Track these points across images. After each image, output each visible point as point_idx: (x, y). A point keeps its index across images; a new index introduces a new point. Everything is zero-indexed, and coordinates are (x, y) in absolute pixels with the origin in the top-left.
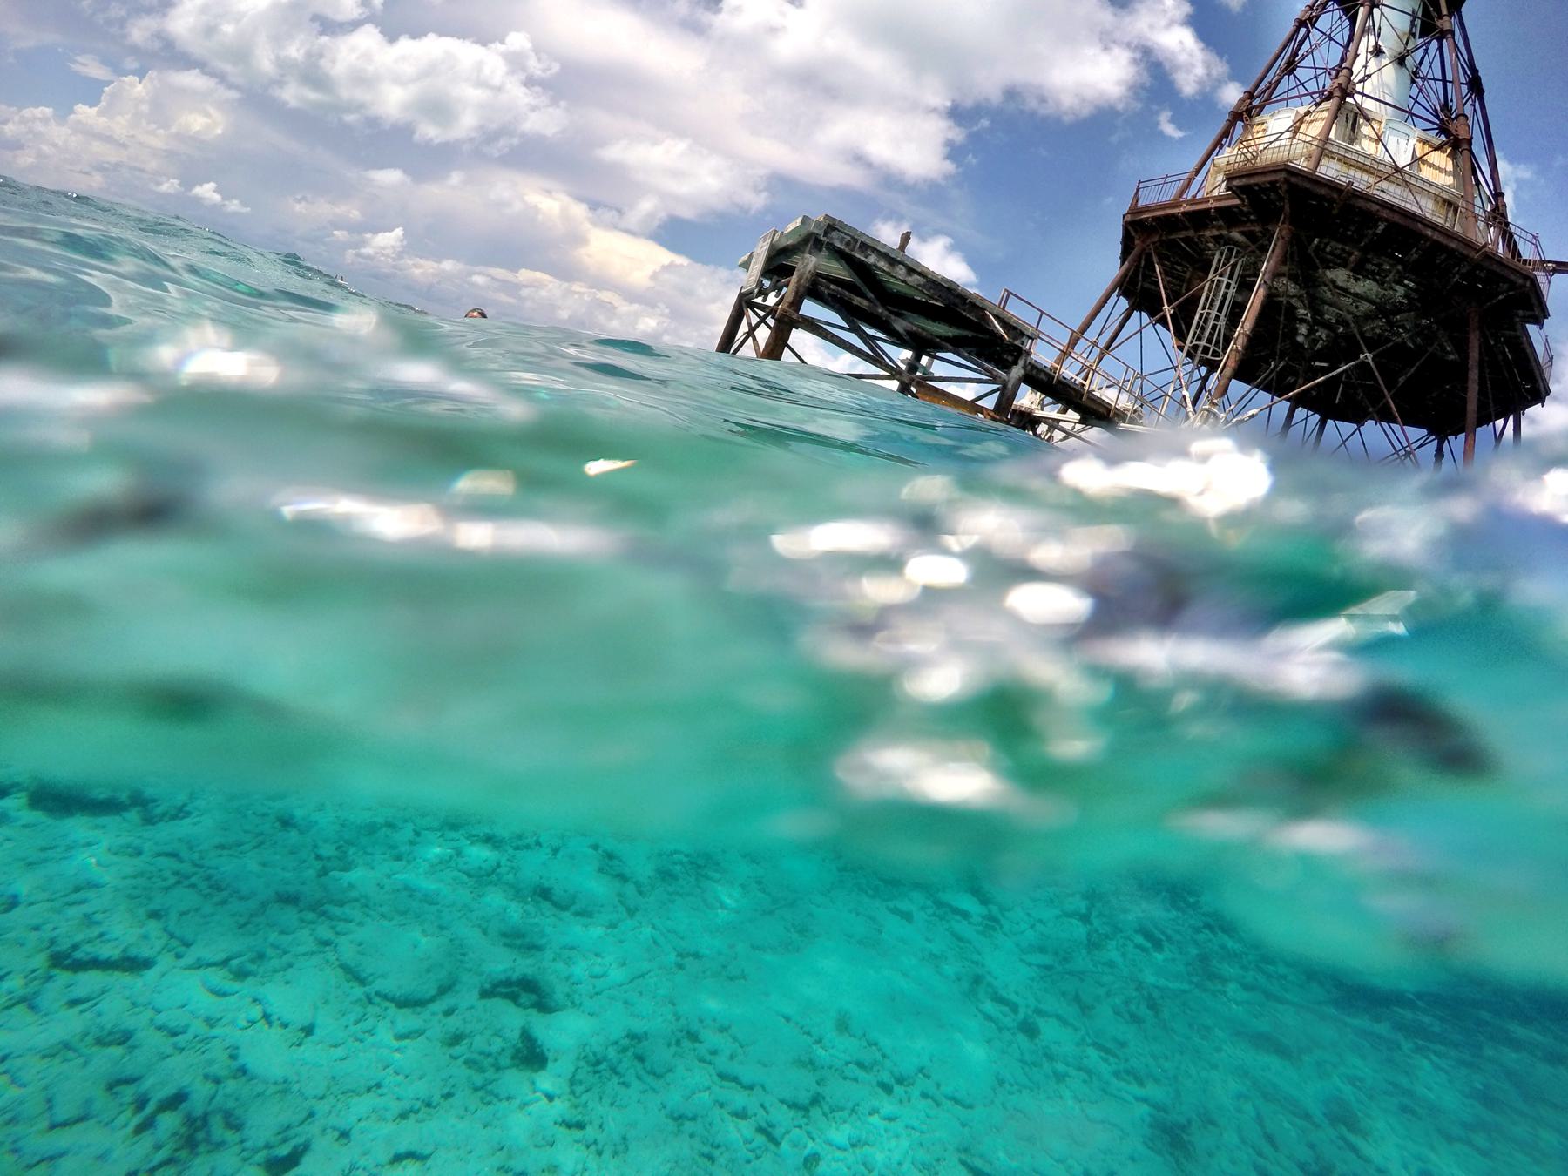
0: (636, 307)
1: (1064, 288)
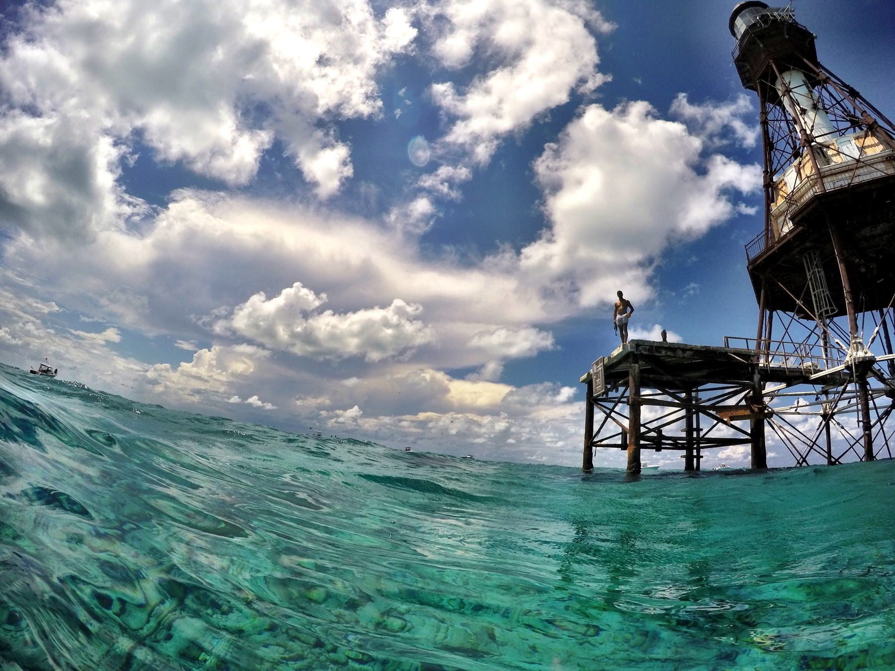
1: (732, 320)
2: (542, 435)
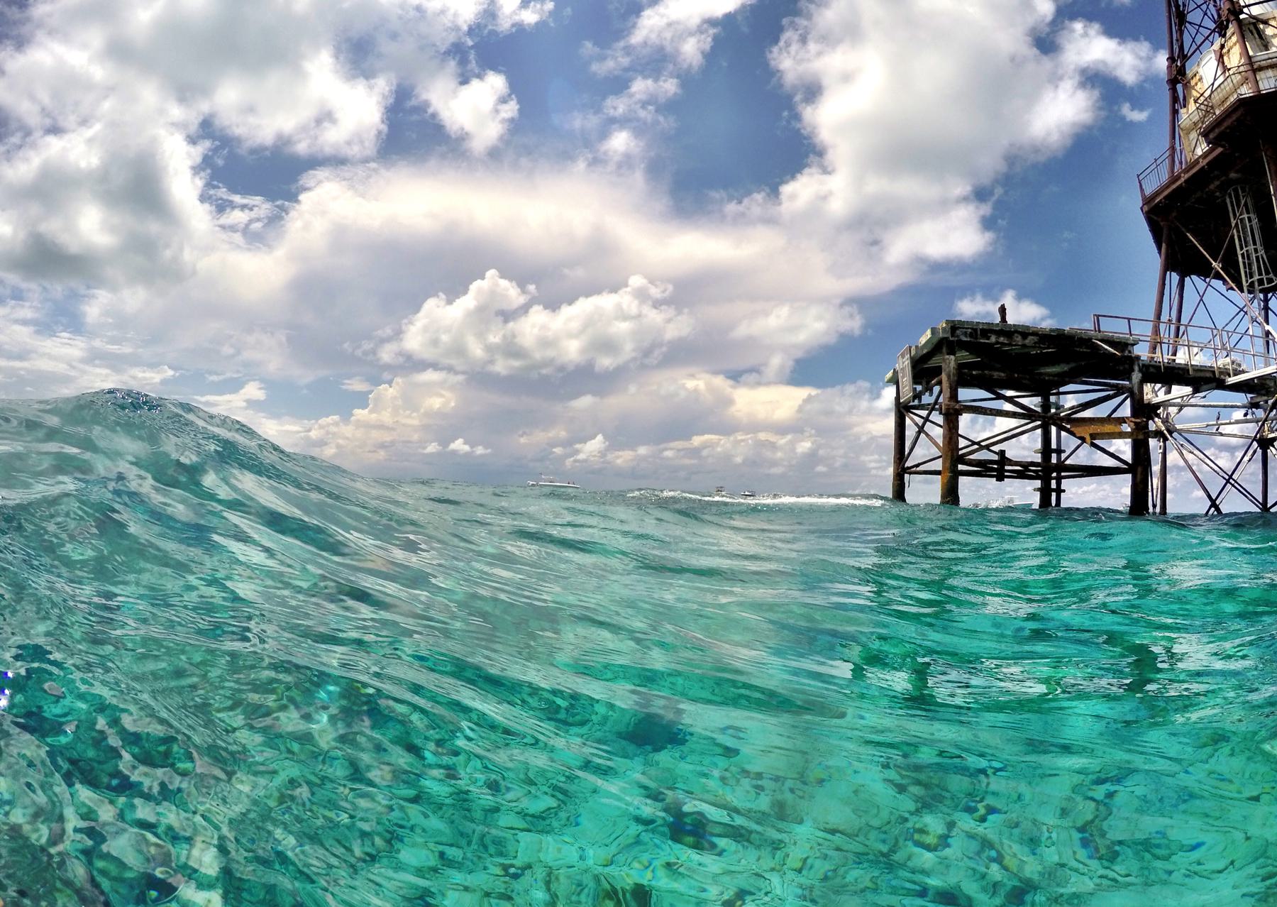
0: (789, 437)
1: (1126, 289)
2: (864, 458)
